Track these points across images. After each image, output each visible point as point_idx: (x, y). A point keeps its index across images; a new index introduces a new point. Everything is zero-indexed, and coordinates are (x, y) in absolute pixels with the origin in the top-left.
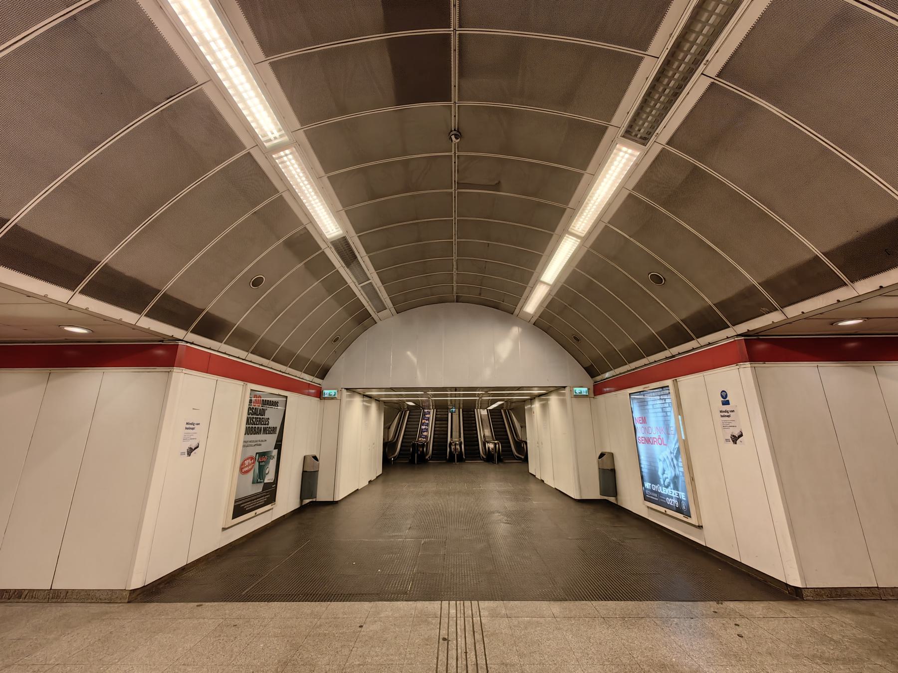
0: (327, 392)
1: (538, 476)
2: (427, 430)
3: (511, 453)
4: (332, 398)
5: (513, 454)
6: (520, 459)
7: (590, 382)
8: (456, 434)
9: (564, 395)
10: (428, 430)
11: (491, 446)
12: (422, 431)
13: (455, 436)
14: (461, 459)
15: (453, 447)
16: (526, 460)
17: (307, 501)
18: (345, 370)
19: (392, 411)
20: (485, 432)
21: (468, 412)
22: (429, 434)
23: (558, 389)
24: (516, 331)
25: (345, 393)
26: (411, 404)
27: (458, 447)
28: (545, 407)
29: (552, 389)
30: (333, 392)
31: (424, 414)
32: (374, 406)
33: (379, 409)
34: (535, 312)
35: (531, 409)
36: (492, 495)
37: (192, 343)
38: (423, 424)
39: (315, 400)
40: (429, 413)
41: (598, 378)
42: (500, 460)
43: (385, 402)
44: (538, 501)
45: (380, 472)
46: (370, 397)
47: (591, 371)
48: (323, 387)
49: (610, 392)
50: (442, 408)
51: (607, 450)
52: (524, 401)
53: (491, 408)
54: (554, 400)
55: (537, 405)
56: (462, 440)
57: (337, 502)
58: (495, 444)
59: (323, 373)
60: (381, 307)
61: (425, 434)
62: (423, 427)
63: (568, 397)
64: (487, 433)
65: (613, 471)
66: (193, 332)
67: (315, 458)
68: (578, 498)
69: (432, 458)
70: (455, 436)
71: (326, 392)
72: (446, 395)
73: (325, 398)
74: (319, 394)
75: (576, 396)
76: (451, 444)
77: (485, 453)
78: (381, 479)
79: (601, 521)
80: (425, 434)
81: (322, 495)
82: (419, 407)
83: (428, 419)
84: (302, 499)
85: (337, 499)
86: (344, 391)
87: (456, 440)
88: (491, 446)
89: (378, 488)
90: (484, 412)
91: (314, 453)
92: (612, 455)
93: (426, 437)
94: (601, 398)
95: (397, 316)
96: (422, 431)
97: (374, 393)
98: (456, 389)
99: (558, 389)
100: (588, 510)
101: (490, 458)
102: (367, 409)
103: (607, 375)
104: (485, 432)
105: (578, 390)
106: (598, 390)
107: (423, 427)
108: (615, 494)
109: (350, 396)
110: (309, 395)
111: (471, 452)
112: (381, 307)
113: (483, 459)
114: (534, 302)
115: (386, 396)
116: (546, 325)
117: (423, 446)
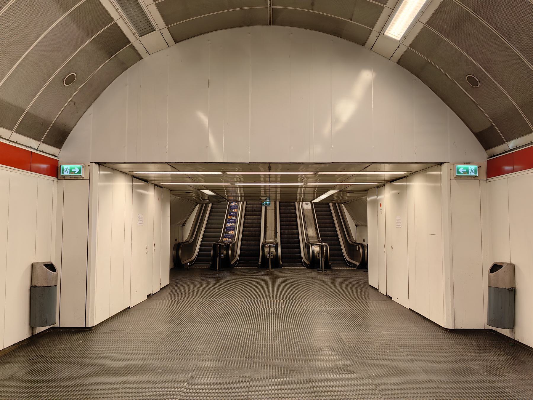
0: (66, 168)
1: (382, 291)
2: (233, 228)
3: (342, 258)
4: (76, 178)
5: (343, 259)
6: (354, 265)
7: (483, 156)
8: (270, 233)
9: (437, 179)
10: (235, 230)
11: (317, 249)
12: (227, 229)
13: (270, 235)
14: (276, 264)
15: (266, 250)
16: (364, 266)
17: (40, 329)
18: (93, 135)
19: (181, 202)
20: (308, 232)
21: (287, 204)
22: (237, 233)
23: (427, 167)
24: (367, 76)
25: (96, 171)
26: (208, 192)
27: (273, 249)
28: (401, 195)
29: (416, 167)
30: (76, 168)
31: (231, 208)
32: (152, 194)
33: (161, 198)
34: (405, 37)
35: (376, 202)
36: (317, 317)
37: (16, 143)
38: (228, 221)
39: (47, 180)
40: (237, 207)
41: (499, 149)
42: (327, 267)
43: (171, 190)
44: (383, 330)
45: (166, 281)
46: (145, 180)
47: (486, 139)
48: (61, 159)
49: (513, 171)
50: (254, 201)
51: (503, 258)
52: (366, 190)
53: (316, 200)
54: (418, 187)
55: (387, 196)
56: (279, 240)
57: (91, 329)
58: (322, 247)
59: (59, 137)
60: (145, 28)
61: (231, 232)
62: (229, 225)
63: (445, 182)
64: (311, 232)
65: (513, 291)
66: (17, 132)
67: (51, 267)
68: (450, 327)
69: (239, 263)
70: (270, 235)
71: (65, 167)
72: (257, 179)
73: (64, 177)
74: (54, 170)
75: (459, 178)
76: (264, 246)
77: (308, 258)
78: (167, 292)
79: (489, 364)
80: (231, 232)
81: (67, 317)
82: (220, 199)
83: (236, 215)
84: (32, 327)
85: (90, 325)
86: (95, 167)
87: (270, 240)
88: (317, 249)
89: (163, 305)
90: (307, 207)
91: (47, 260)
92: (513, 267)
93: (233, 237)
94: (500, 181)
95: (176, 48)
96: (227, 229)
97: (152, 173)
98: (270, 166)
99: (427, 167)
100: (467, 349)
101: (314, 263)
102: (141, 198)
103: (512, 144)
104: (308, 232)
105: (462, 168)
106: (494, 169)
107: (229, 225)
108: (512, 324)
109: (108, 178)
110: (38, 171)
111: (290, 255)
112: (145, 28)
113: (305, 265)
114: (398, 27)
115: (174, 178)
116: (420, 65)
117: (227, 248)
